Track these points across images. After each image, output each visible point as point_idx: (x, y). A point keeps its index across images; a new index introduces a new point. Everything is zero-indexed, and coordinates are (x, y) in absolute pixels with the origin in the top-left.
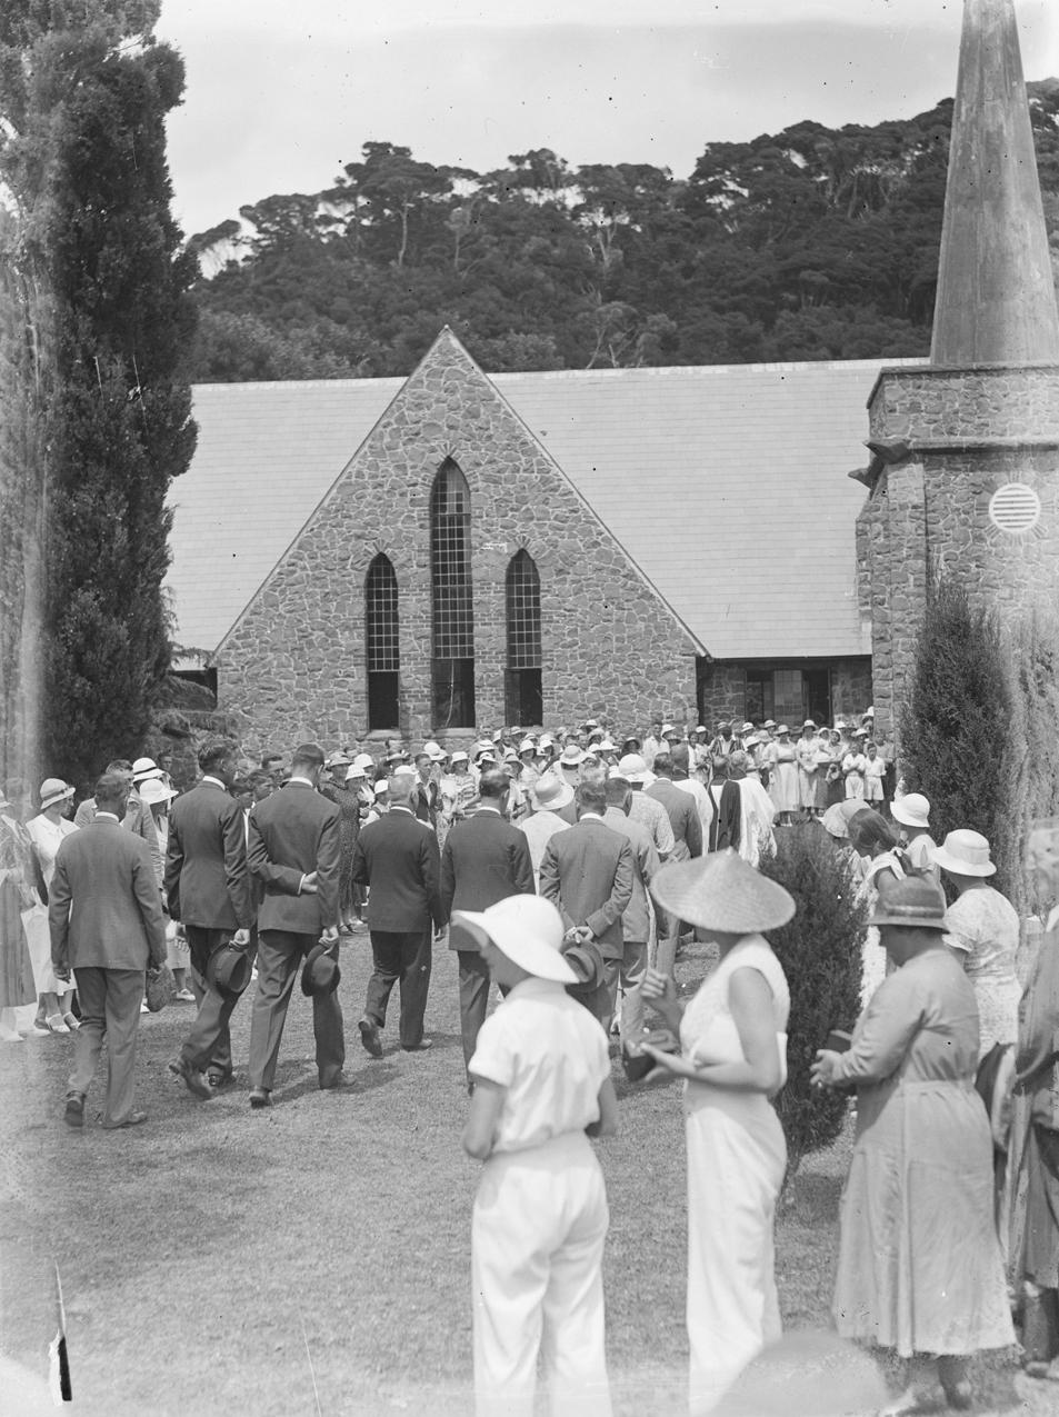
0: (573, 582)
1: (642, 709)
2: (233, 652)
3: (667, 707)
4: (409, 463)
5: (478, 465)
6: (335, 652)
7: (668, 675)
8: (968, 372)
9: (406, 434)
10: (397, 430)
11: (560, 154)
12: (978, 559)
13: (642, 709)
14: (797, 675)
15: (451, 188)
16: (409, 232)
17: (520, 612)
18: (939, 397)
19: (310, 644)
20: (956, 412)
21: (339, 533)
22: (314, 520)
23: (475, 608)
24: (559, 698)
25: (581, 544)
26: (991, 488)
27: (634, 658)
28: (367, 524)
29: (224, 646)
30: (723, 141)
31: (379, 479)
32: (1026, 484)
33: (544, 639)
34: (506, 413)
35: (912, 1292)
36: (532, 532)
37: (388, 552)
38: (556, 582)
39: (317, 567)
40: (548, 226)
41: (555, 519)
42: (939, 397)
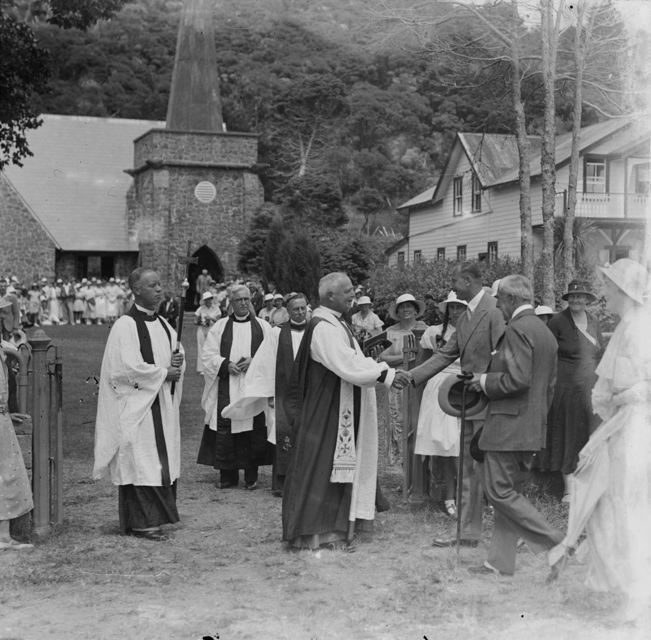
1: (29, 272)
7: (42, 257)
8: (188, 133)
12: (189, 212)
13: (29, 272)
14: (99, 259)
16: (204, 129)
18: (176, 143)
20: (183, 150)
26: (196, 183)
27: (26, 248)
35: (306, 376)
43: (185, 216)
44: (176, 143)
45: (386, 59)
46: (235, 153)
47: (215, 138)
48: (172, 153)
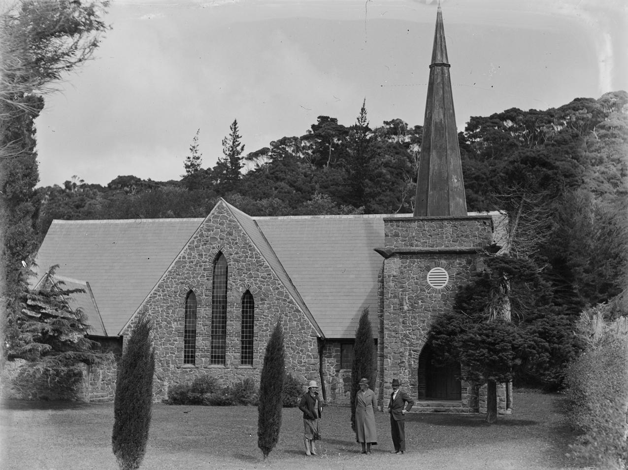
0: (268, 304)
2: (130, 329)
3: (304, 358)
4: (204, 253)
5: (231, 254)
6: (170, 331)
9: (203, 241)
10: (200, 240)
11: (405, 120)
12: (422, 299)
15: (462, 133)
17: (247, 316)
19: (161, 327)
20: (414, 237)
21: (175, 281)
22: (165, 275)
23: (227, 314)
24: (260, 353)
25: (271, 289)
28: (186, 278)
29: (126, 327)
30: (478, 116)
31: (192, 259)
32: (443, 268)
33: (255, 328)
34: (243, 233)
36: (252, 283)
37: (194, 289)
38: (261, 304)
39: (165, 295)
40: (394, 151)
41: (262, 277)
42: (407, 231)
43: (418, 303)
44: (407, 231)
45: (43, 101)
46: (467, 236)
47: (446, 223)
48: (403, 241)
